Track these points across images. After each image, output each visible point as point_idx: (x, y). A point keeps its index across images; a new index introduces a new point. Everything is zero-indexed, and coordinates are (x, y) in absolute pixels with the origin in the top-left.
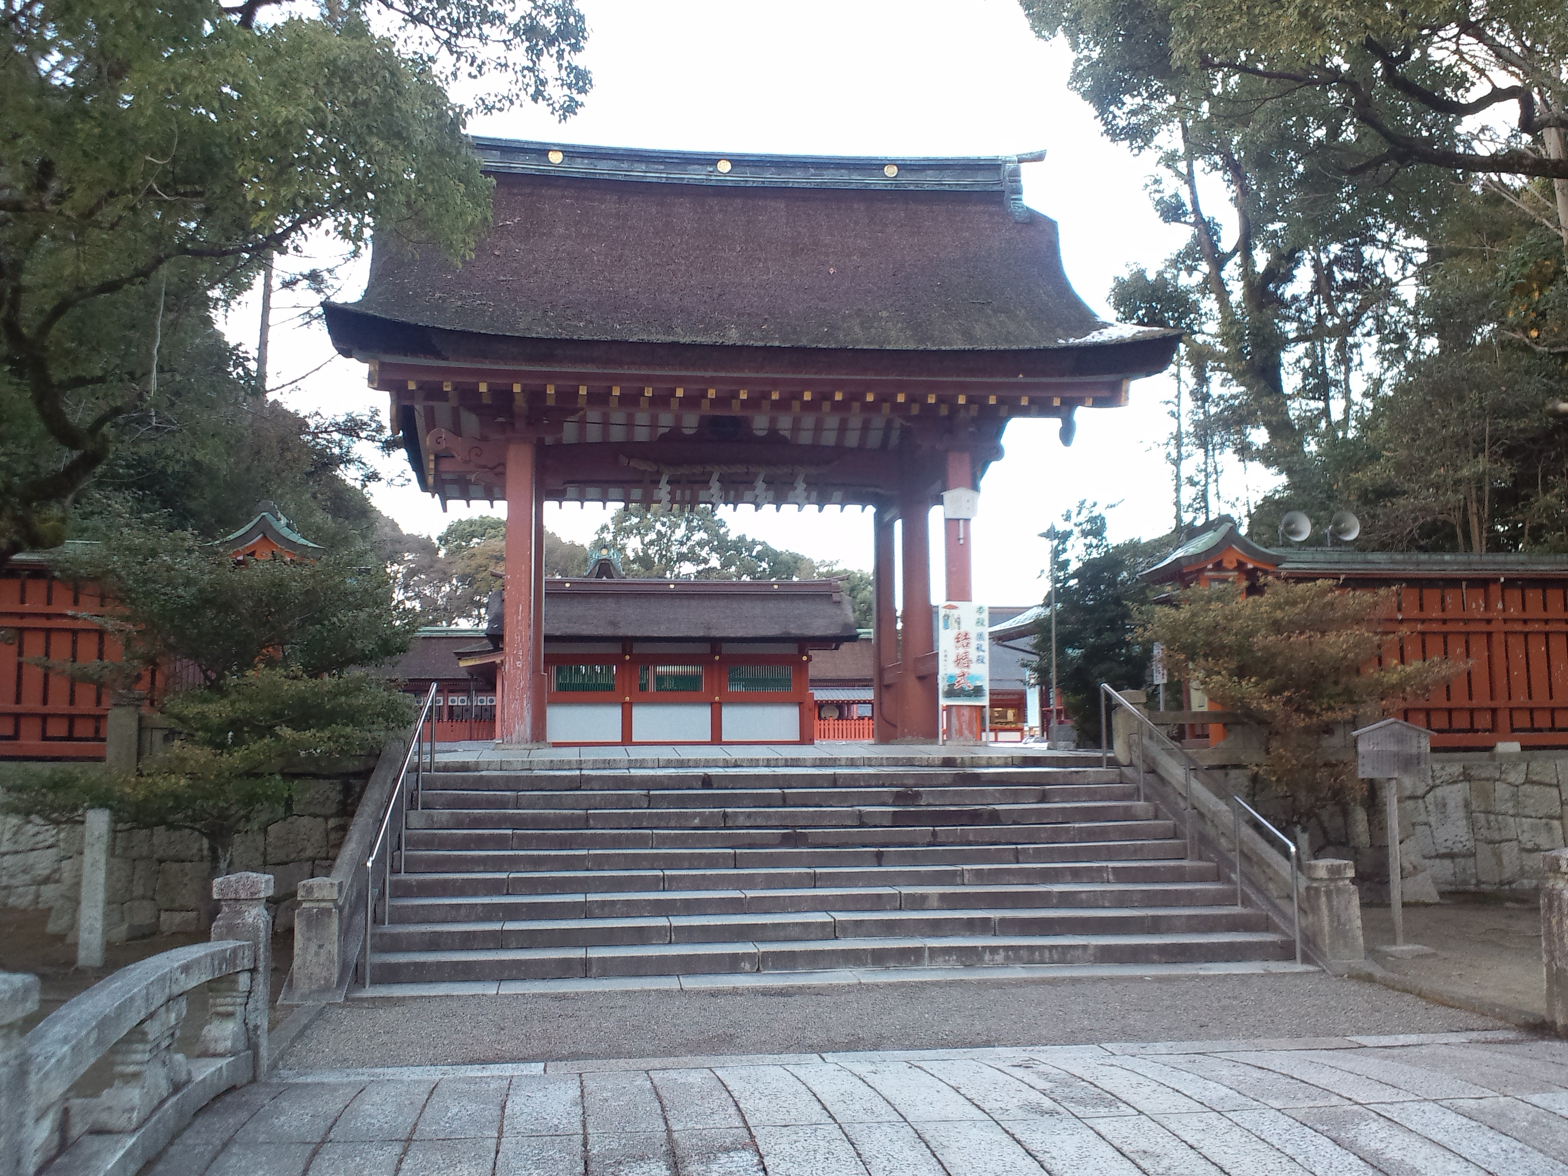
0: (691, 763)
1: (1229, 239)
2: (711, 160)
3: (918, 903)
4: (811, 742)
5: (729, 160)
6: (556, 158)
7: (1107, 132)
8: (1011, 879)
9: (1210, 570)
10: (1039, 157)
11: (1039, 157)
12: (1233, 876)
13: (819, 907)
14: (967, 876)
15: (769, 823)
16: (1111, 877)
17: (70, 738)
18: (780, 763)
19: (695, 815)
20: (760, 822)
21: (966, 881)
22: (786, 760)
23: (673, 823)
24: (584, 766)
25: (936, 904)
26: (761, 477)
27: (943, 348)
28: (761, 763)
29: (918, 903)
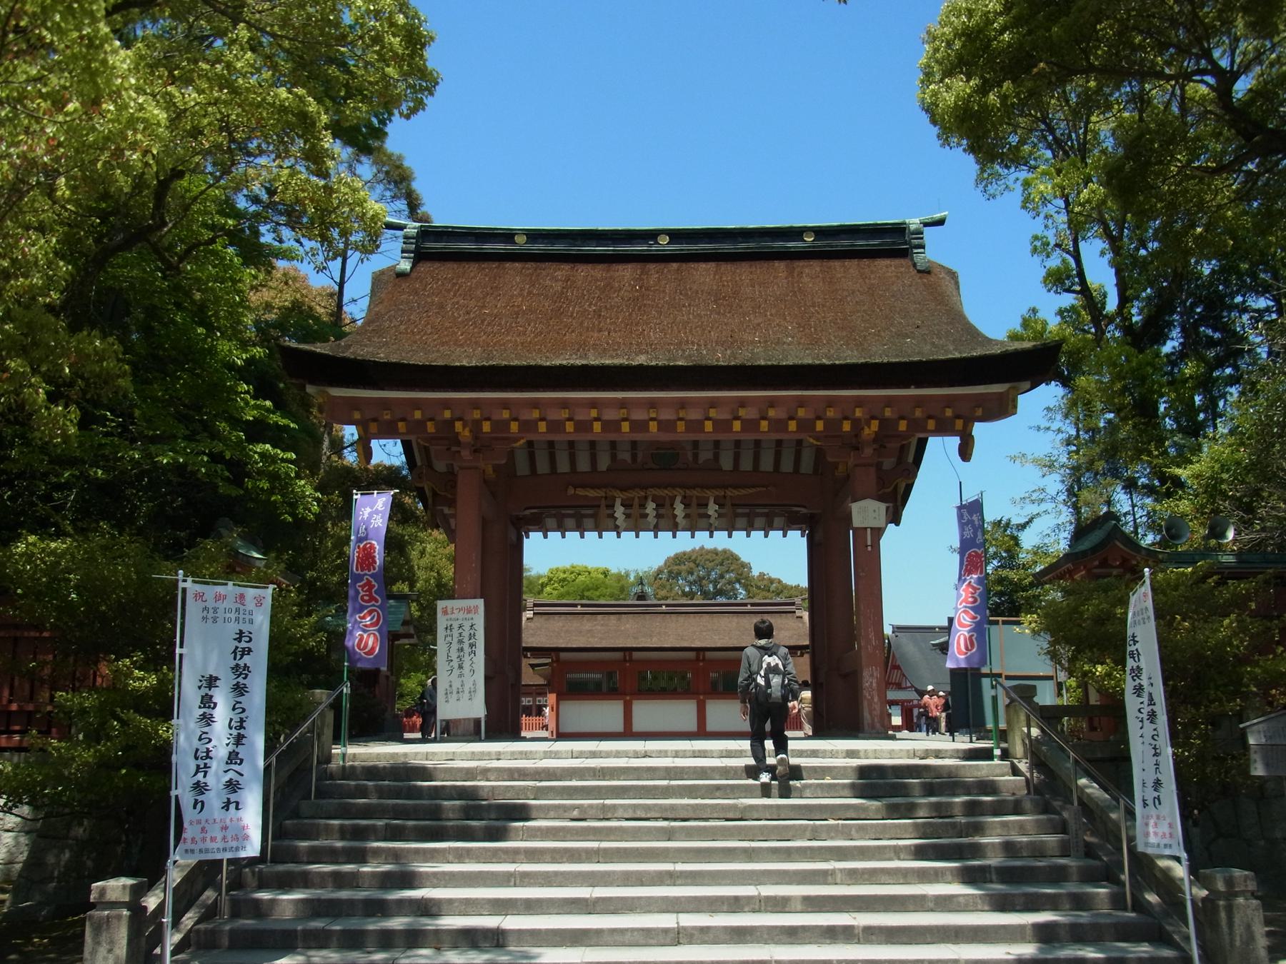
0: (603, 755)
1: (1112, 305)
2: (652, 235)
3: (779, 904)
4: (513, 734)
5: (668, 234)
6: (520, 239)
7: (1048, 653)
8: (883, 879)
9: (1096, 567)
10: (940, 222)
11: (940, 222)
12: (1123, 877)
13: (670, 909)
14: (839, 876)
15: (649, 816)
16: (994, 877)
17: (628, 733)
18: (688, 755)
19: (574, 807)
20: (640, 814)
21: (838, 881)
22: (694, 751)
23: (552, 814)
24: (502, 757)
25: (799, 907)
26: (678, 499)
27: (837, 362)
28: (669, 754)
29: (779, 904)
